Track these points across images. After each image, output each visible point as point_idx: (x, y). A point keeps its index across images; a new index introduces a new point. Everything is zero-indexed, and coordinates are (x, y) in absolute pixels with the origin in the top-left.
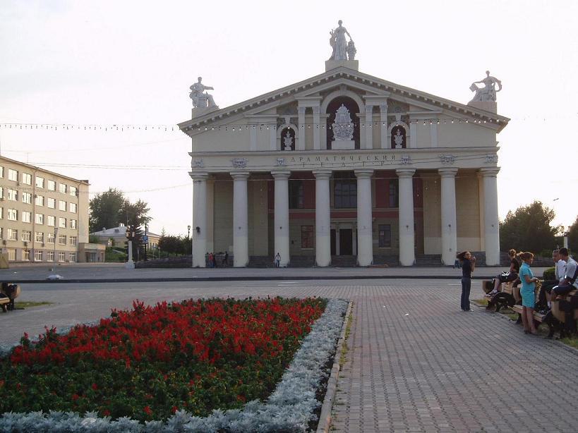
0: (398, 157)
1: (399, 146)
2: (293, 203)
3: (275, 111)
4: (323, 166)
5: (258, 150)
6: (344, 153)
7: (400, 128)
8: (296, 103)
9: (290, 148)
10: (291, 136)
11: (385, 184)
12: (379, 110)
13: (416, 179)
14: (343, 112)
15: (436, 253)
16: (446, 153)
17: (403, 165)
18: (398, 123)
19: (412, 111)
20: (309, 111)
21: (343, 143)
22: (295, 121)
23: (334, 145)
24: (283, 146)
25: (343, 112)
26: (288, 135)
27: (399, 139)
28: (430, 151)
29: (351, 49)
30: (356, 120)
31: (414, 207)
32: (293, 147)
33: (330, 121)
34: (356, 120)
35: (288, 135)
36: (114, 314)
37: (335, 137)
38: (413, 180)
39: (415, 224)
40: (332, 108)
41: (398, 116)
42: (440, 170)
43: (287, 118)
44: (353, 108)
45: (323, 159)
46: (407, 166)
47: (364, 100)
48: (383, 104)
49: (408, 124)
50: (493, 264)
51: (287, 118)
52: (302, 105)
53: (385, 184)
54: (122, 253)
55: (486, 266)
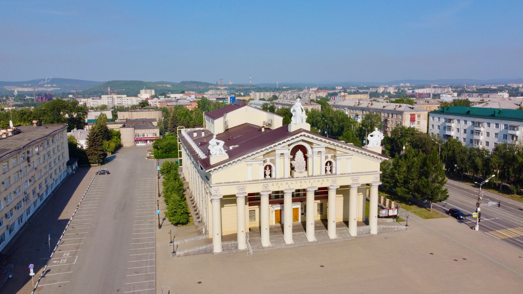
0: (330, 179)
1: (329, 173)
3: (262, 157)
4: (289, 188)
5: (246, 180)
7: (330, 163)
13: (502, 190)
14: (299, 153)
17: (332, 184)
18: (329, 159)
24: (265, 175)
25: (299, 153)
26: (268, 168)
27: (328, 168)
29: (41, 259)
30: (306, 158)
32: (270, 175)
34: (306, 158)
35: (268, 168)
36: (100, 97)
41: (330, 156)
43: (268, 159)
44: (304, 150)
45: (290, 182)
47: (312, 148)
48: (323, 150)
49: (335, 160)
50: (232, 181)
51: (268, 159)
52: (278, 152)
55: (260, 227)
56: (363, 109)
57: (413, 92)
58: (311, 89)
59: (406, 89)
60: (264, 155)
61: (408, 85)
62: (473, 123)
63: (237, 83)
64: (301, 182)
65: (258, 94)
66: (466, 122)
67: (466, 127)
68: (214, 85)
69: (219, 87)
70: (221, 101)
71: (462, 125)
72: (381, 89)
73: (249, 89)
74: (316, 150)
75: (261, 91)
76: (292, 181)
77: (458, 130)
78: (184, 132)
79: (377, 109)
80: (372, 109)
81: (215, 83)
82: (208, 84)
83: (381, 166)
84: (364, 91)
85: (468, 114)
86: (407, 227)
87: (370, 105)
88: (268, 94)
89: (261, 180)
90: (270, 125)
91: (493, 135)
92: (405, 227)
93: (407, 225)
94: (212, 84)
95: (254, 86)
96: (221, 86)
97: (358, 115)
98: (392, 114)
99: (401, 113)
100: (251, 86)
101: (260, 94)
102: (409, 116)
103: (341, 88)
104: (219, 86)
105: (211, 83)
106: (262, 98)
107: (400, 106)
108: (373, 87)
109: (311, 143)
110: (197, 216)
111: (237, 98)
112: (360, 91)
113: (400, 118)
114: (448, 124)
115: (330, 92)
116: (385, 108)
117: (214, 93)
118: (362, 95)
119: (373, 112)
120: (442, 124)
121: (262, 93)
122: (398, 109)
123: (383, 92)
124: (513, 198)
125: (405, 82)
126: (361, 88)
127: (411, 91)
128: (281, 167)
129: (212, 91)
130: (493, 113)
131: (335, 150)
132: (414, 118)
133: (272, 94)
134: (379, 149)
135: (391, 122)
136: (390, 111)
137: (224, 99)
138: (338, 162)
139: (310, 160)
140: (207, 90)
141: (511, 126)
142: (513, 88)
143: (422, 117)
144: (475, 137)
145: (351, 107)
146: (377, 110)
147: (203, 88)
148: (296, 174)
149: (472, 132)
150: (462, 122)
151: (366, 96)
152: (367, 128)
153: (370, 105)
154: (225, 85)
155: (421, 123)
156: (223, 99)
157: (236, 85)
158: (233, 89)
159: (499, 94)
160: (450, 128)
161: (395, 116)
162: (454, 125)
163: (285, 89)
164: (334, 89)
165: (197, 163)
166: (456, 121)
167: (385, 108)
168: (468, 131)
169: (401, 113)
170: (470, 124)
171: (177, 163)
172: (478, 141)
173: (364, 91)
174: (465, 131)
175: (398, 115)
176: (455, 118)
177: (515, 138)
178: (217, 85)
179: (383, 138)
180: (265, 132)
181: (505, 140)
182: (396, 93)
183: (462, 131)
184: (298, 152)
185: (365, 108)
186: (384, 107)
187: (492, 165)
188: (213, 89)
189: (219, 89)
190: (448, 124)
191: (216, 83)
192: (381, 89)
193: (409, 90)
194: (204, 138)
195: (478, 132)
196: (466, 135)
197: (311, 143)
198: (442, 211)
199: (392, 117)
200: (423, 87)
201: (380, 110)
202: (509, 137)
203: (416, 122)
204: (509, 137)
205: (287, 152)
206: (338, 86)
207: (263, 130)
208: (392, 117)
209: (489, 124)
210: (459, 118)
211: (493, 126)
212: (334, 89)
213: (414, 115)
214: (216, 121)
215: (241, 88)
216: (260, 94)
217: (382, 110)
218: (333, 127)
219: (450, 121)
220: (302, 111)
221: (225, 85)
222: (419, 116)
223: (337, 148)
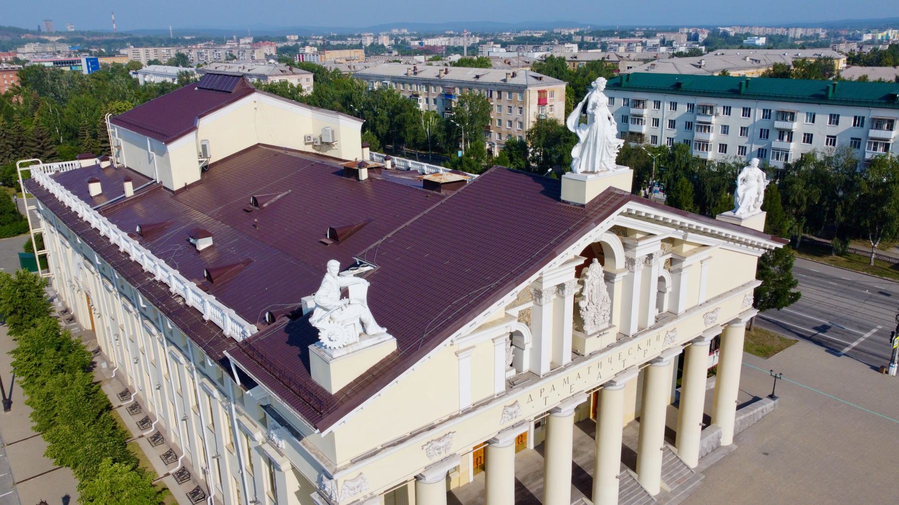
50: (406, 432)
56: (427, 83)
57: (421, 44)
58: (242, 41)
59: (408, 39)
61: (405, 31)
62: (691, 106)
63: (85, 28)
64: (600, 365)
65: (142, 51)
66: (674, 106)
67: (675, 116)
68: (33, 33)
69: (46, 37)
70: (67, 69)
71: (666, 113)
72: (368, 38)
73: (114, 41)
74: (642, 250)
75: (141, 46)
77: (656, 122)
78: (42, 173)
79: (463, 82)
80: (451, 81)
81: (36, 28)
82: (18, 31)
83: (760, 267)
84: (339, 42)
85: (821, 98)
86: (777, 401)
87: (442, 74)
88: (164, 50)
89: (500, 396)
90: (329, 145)
91: (735, 130)
92: (772, 403)
93: (772, 397)
94: (27, 31)
95: (122, 34)
96: (50, 34)
97: (417, 96)
98: (499, 92)
99: (521, 89)
100: (116, 34)
101: (147, 52)
102: (537, 95)
103: (297, 37)
104: (44, 34)
105: (24, 27)
106: (152, 58)
107: (514, 75)
108: (352, 36)
110: (67, 316)
111: (101, 60)
112: (332, 42)
113: (519, 98)
114: (634, 111)
115: (280, 45)
116: (481, 80)
117: (40, 49)
118: (352, 51)
119: (454, 88)
120: (680, 118)
121: (151, 50)
122: (511, 81)
123: (372, 45)
124: (837, 265)
125: (400, 26)
126: (333, 38)
127: (417, 43)
129: (33, 45)
130: (738, 88)
132: (545, 99)
133: (173, 52)
134: (757, 220)
135: (496, 108)
136: (495, 85)
137: (73, 62)
138: (685, 276)
140: (22, 44)
141: (778, 112)
142: (564, 36)
143: (556, 95)
144: (699, 136)
145: (400, 78)
146: (461, 84)
147: (7, 38)
148: (591, 345)
149: (689, 125)
150: (667, 106)
151: (360, 53)
152: (464, 123)
153: (442, 74)
154: (57, 34)
155: (556, 107)
156: (71, 63)
157: (82, 33)
158: (79, 41)
159: (566, 45)
160: (638, 119)
161: (505, 95)
162: (648, 112)
163: (189, 40)
164: (285, 40)
165: (225, 363)
166: (650, 104)
167: (481, 80)
168: (680, 124)
169: (521, 89)
170: (683, 108)
171: (29, 246)
172: (704, 145)
173: (339, 42)
174: (672, 124)
175: (406, 85)
176: (719, 105)
177: (786, 137)
178: (39, 32)
180: (370, 178)
181: (763, 141)
182: (392, 45)
183: (666, 124)
185: (434, 80)
186: (477, 77)
187: (794, 201)
188: (30, 41)
189: (46, 41)
190: (634, 111)
191: (36, 29)
192: (368, 38)
193: (412, 40)
194: (133, 200)
195: (706, 127)
196: (675, 130)
198: (765, 325)
199: (500, 98)
200: (433, 36)
201: (469, 83)
202: (774, 135)
203: (547, 107)
204: (774, 135)
206: (290, 35)
207: (364, 174)
208: (500, 98)
209: (658, 104)
210: (658, 97)
211: (737, 112)
212: (285, 40)
213: (544, 91)
214: (172, 147)
215: (95, 38)
216: (147, 52)
217: (475, 83)
218: (378, 123)
219: (706, 109)
221: (57, 34)
222: (552, 95)
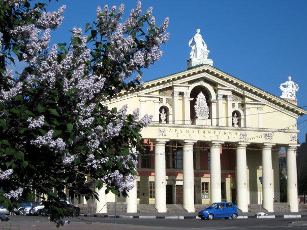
2: (223, 167)
4: (191, 136)
6: (205, 128)
8: (171, 88)
9: (165, 122)
10: (165, 113)
11: (229, 152)
12: (227, 97)
14: (201, 97)
15: (169, 205)
16: (270, 132)
17: (242, 138)
19: (247, 100)
20: (181, 94)
21: (201, 121)
22: (171, 102)
23: (198, 122)
25: (201, 97)
27: (163, 117)
28: (258, 130)
31: (221, 169)
32: (167, 120)
33: (193, 104)
35: (163, 112)
37: (197, 115)
38: (272, 151)
39: (194, 186)
40: (194, 94)
41: (237, 104)
42: (157, 140)
45: (191, 130)
46: (164, 137)
47: (216, 91)
49: (244, 110)
52: (177, 90)
53: (229, 152)
54: (7, 216)
60: (160, 91)
74: (221, 93)
76: (182, 129)
109: (214, 84)
128: (180, 109)
131: (243, 97)
138: (247, 112)
139: (214, 106)
179: (297, 90)
184: (200, 94)
197: (214, 84)
205: (188, 91)
220: (204, 44)
223: (247, 93)
